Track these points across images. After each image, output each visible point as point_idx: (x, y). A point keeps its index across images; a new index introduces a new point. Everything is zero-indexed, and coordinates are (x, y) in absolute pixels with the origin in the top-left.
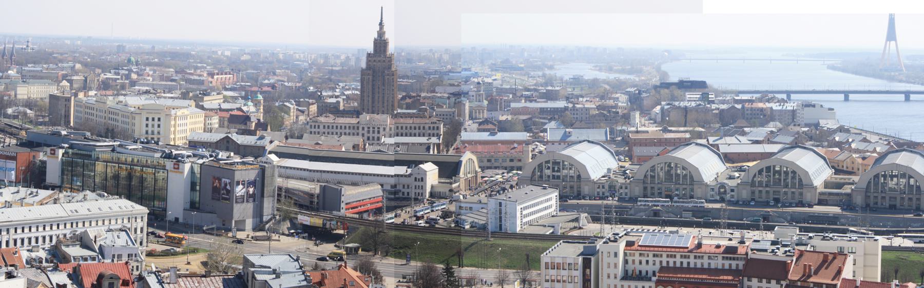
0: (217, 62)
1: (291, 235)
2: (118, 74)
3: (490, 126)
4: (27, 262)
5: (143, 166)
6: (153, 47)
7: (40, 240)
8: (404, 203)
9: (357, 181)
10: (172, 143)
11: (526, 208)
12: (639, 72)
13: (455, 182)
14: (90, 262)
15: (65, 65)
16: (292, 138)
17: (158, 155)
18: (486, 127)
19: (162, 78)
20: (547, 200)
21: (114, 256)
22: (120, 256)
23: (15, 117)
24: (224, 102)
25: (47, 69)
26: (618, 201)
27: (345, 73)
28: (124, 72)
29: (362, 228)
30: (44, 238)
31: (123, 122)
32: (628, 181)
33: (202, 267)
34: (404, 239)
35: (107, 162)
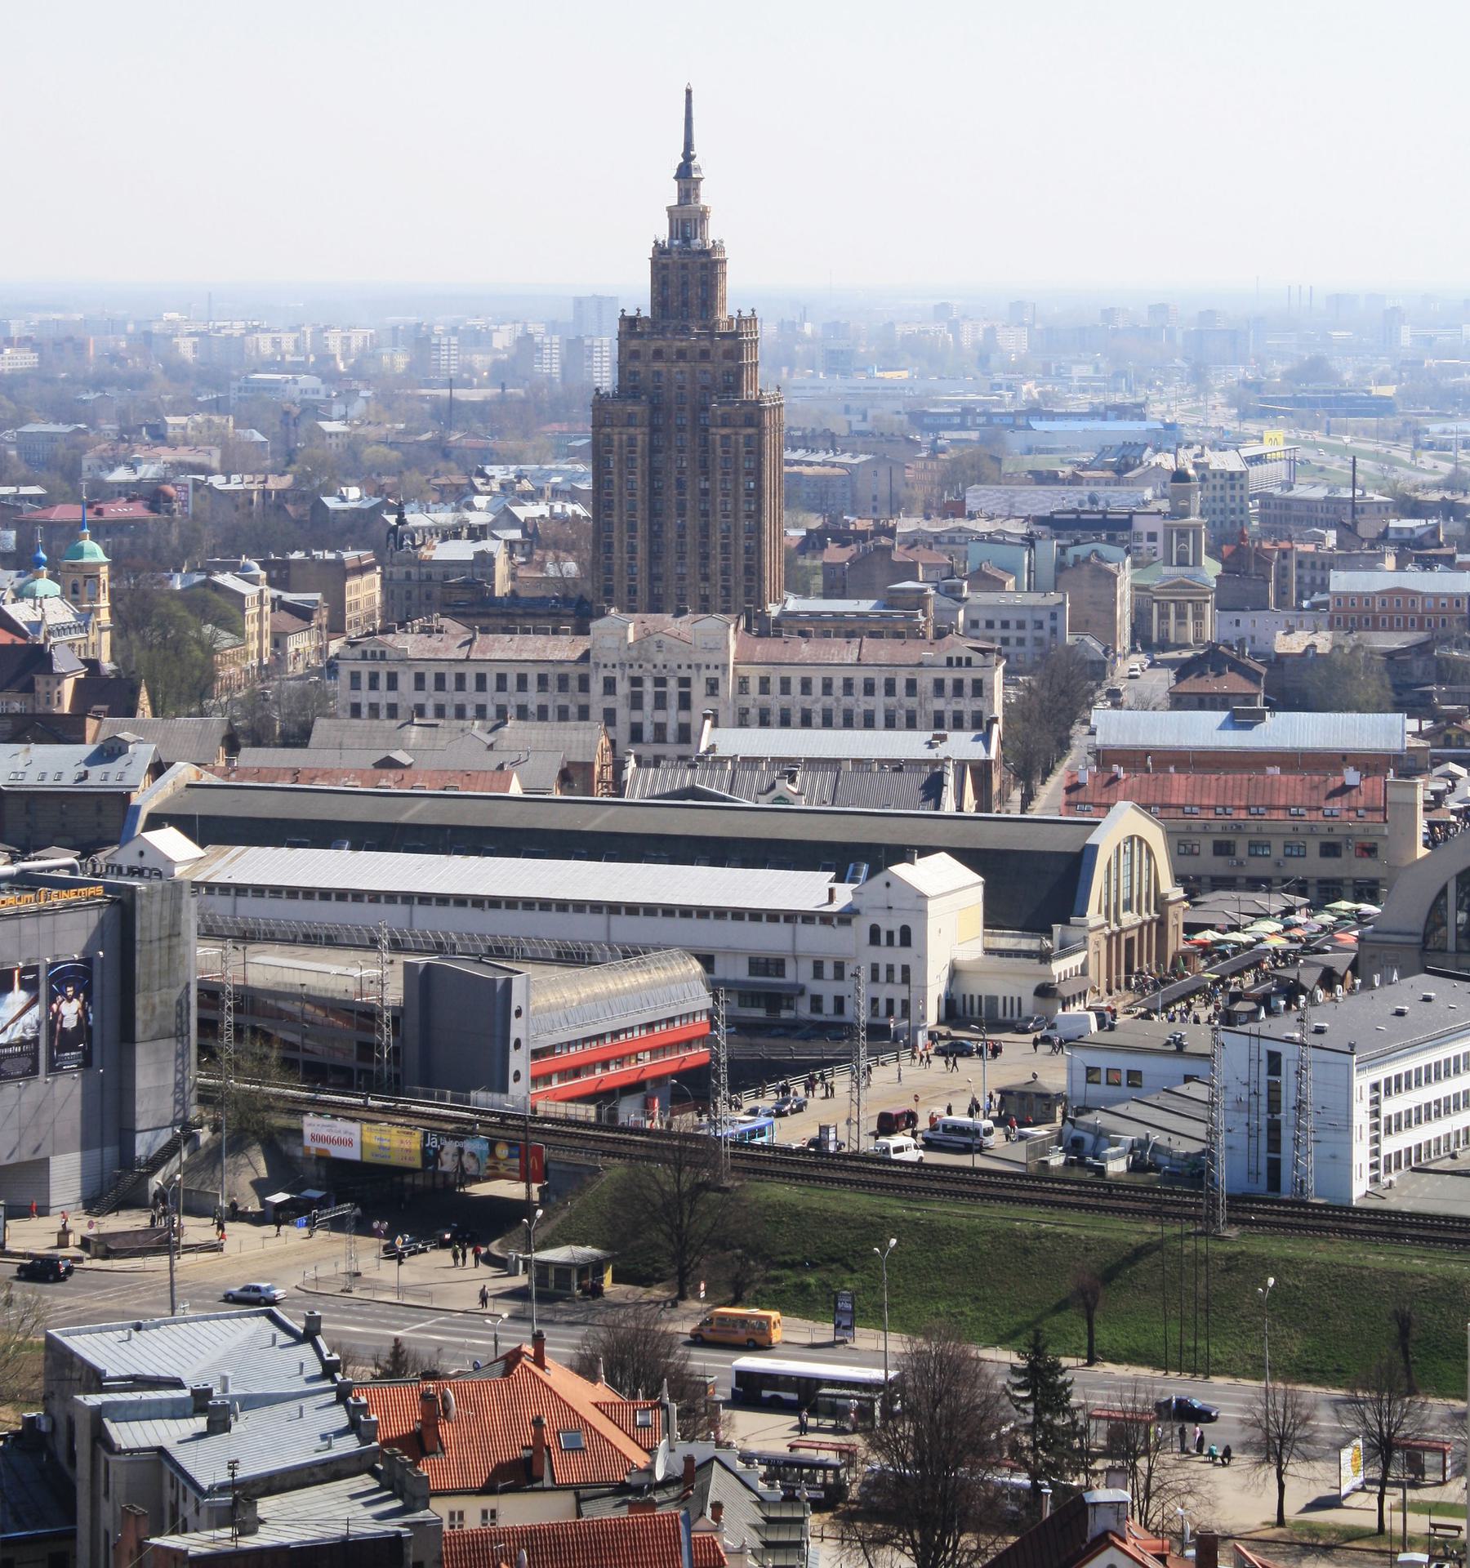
1: (276, 1217)
3: (1231, 683)
9: (587, 939)
11: (1396, 1085)
13: (1066, 949)
16: (257, 742)
27: (514, 416)
29: (616, 1170)
34: (825, 1220)
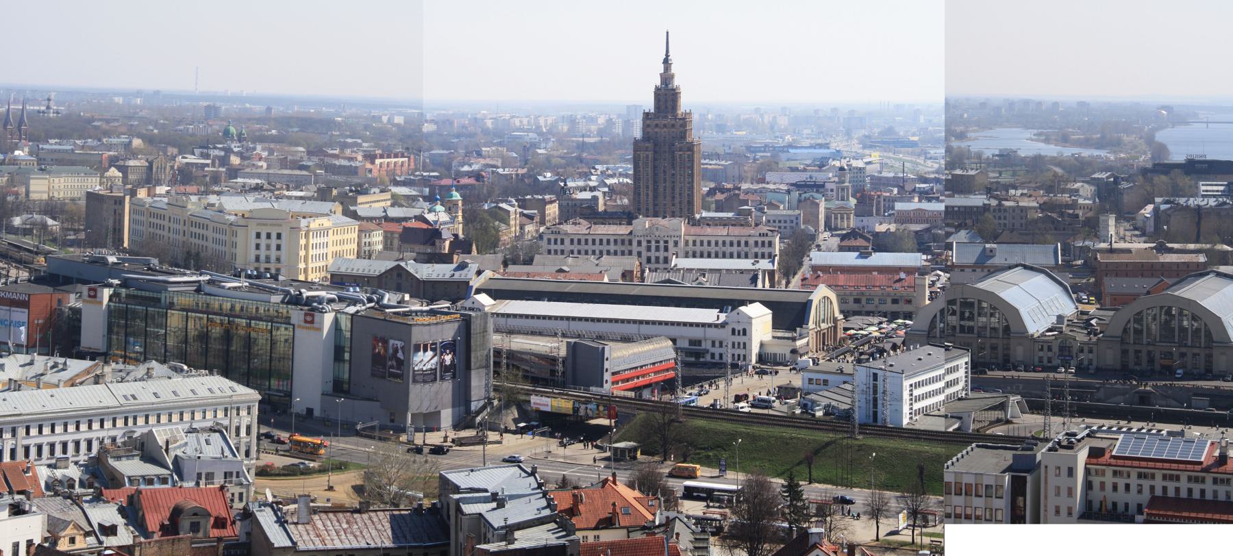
0: (380, 136)
1: (521, 431)
2: (207, 156)
3: (860, 242)
4: (48, 487)
5: (251, 319)
6: (269, 109)
7: (71, 447)
8: (714, 372)
9: (631, 333)
10: (302, 278)
12: (1115, 144)
13: (801, 337)
14: (157, 486)
15: (114, 140)
16: (514, 263)
17: (277, 299)
18: (853, 243)
19: (284, 163)
20: (950, 371)
21: (199, 476)
22: (210, 477)
23: (26, 232)
24: (393, 205)
25: (83, 147)
26: (1076, 374)
27: (605, 148)
28: (217, 152)
29: (641, 415)
30: (77, 443)
31: (215, 241)
32: (1094, 339)
33: (354, 496)
34: (716, 433)
35: (187, 310)
